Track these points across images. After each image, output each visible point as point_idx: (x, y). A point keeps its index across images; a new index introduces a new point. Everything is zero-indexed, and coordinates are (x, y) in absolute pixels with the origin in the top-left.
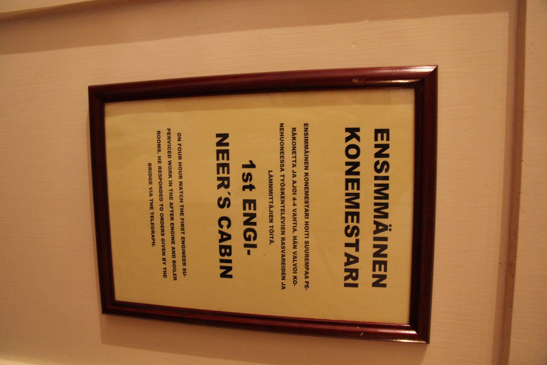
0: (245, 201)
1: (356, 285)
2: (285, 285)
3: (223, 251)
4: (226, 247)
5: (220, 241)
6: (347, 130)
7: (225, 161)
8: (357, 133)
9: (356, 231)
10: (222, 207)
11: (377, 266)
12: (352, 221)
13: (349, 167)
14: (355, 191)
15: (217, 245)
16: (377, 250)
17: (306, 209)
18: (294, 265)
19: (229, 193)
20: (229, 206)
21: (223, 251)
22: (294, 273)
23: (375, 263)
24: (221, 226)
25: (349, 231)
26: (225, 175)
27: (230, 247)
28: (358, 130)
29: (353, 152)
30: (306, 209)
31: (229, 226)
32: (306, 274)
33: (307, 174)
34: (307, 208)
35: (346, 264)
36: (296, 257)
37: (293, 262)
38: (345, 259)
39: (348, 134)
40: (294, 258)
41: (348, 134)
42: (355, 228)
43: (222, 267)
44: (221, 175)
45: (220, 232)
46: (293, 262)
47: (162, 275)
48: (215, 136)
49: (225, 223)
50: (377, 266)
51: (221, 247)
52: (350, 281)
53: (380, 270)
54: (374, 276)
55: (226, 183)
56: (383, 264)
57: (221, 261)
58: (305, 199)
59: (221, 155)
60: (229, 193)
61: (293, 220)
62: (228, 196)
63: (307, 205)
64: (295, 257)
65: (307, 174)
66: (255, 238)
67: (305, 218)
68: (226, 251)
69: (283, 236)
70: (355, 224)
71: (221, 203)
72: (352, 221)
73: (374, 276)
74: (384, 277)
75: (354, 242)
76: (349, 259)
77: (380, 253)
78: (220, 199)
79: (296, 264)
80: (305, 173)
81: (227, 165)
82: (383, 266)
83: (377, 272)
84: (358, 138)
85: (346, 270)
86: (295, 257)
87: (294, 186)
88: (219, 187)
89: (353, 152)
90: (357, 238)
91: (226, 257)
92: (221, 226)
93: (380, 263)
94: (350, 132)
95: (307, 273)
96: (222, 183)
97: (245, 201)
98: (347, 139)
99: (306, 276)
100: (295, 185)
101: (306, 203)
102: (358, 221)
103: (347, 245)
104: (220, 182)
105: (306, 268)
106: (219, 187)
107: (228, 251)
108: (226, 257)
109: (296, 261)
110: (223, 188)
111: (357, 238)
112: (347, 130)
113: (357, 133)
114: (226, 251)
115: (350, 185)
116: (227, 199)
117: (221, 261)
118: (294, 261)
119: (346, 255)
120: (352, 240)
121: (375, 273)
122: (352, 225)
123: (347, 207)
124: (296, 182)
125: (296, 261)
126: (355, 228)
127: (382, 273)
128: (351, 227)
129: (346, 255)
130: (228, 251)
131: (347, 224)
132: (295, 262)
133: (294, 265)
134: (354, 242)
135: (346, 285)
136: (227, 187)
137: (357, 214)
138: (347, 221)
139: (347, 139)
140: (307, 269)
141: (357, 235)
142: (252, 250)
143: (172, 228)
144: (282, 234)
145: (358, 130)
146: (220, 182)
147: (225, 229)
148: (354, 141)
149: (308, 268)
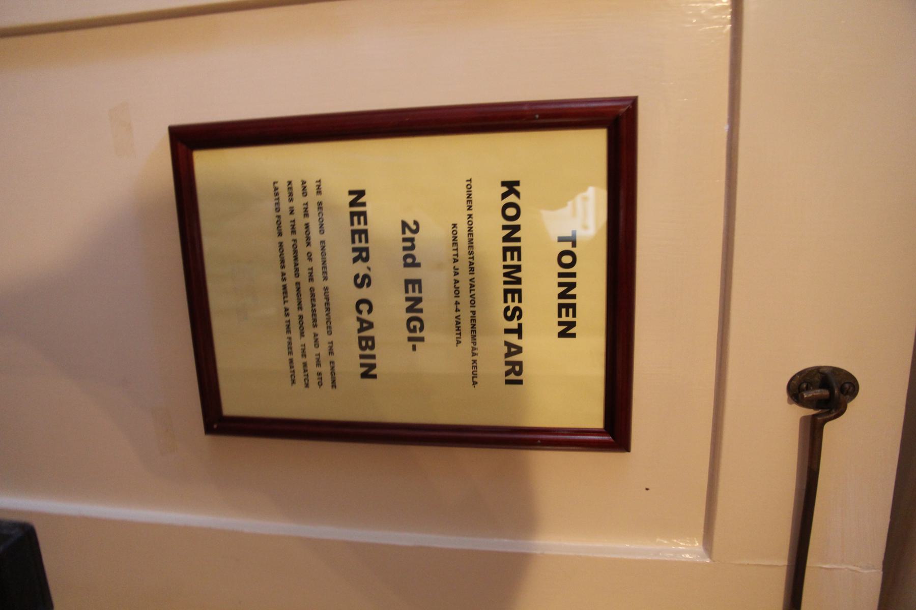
0: (407, 282)
1: (520, 382)
2: (458, 269)
3: (364, 343)
4: (367, 339)
5: (360, 331)
6: (504, 184)
7: (362, 227)
8: (516, 188)
9: (518, 313)
10: (360, 286)
11: (564, 311)
12: (513, 300)
13: (507, 232)
14: (515, 262)
15: (355, 336)
16: (563, 289)
17: (470, 262)
18: (471, 296)
19: (369, 269)
20: (369, 285)
21: (364, 343)
22: (471, 307)
23: (560, 306)
24: (360, 312)
25: (509, 313)
26: (363, 245)
27: (372, 339)
28: (517, 183)
29: (511, 212)
30: (470, 262)
31: (370, 311)
32: (473, 350)
33: (470, 216)
34: (471, 260)
35: (507, 355)
36: (474, 286)
37: (470, 292)
38: (505, 350)
39: (505, 189)
40: (471, 287)
41: (505, 189)
42: (517, 309)
43: (362, 365)
44: (357, 245)
45: (359, 319)
46: (470, 292)
47: (290, 231)
48: (347, 193)
49: (364, 307)
50: (564, 311)
51: (361, 339)
52: (512, 377)
53: (567, 315)
54: (560, 324)
55: (364, 255)
56: (571, 308)
57: (362, 357)
58: (469, 249)
59: (356, 218)
60: (369, 269)
61: (456, 330)
62: (367, 272)
63: (471, 256)
64: (472, 286)
65: (470, 216)
66: (422, 329)
67: (470, 274)
68: (367, 343)
69: (470, 212)
70: (516, 304)
71: (359, 281)
72: (513, 300)
73: (560, 324)
74: (572, 325)
75: (516, 327)
76: (511, 350)
77: (568, 293)
78: (357, 276)
79: (474, 295)
80: (468, 215)
81: (365, 232)
82: (571, 310)
83: (564, 318)
84: (518, 194)
85: (507, 363)
86: (472, 286)
87: (457, 286)
88: (355, 260)
89: (511, 212)
90: (520, 321)
91: (368, 352)
92: (360, 312)
93: (567, 306)
94: (508, 187)
95: (474, 349)
96: (359, 255)
97: (407, 282)
98: (504, 196)
99: (473, 353)
100: (457, 285)
101: (470, 254)
102: (520, 301)
103: (508, 331)
104: (357, 254)
105: (473, 343)
106: (355, 260)
107: (370, 343)
108: (368, 352)
109: (474, 290)
110: (360, 262)
111: (520, 321)
112: (504, 184)
113: (516, 188)
114: (367, 343)
115: (509, 254)
116: (366, 276)
117: (362, 357)
118: (471, 291)
119: (507, 343)
120: (514, 324)
121: (560, 320)
122: (512, 305)
123: (505, 283)
124: (458, 282)
125: (474, 290)
126: (517, 309)
127: (570, 319)
128: (511, 309)
129: (507, 343)
130: (370, 343)
131: (506, 305)
132: (473, 293)
133: (471, 296)
134: (516, 327)
135: (508, 382)
136: (366, 259)
137: (519, 291)
138: (506, 301)
139: (504, 196)
140: (475, 343)
141: (519, 317)
142: (418, 344)
143: (298, 289)
144: (468, 209)
145: (517, 183)
146: (357, 254)
147: (365, 316)
148: (512, 198)
149: (476, 343)
